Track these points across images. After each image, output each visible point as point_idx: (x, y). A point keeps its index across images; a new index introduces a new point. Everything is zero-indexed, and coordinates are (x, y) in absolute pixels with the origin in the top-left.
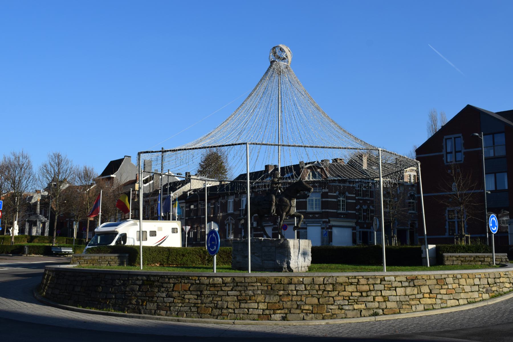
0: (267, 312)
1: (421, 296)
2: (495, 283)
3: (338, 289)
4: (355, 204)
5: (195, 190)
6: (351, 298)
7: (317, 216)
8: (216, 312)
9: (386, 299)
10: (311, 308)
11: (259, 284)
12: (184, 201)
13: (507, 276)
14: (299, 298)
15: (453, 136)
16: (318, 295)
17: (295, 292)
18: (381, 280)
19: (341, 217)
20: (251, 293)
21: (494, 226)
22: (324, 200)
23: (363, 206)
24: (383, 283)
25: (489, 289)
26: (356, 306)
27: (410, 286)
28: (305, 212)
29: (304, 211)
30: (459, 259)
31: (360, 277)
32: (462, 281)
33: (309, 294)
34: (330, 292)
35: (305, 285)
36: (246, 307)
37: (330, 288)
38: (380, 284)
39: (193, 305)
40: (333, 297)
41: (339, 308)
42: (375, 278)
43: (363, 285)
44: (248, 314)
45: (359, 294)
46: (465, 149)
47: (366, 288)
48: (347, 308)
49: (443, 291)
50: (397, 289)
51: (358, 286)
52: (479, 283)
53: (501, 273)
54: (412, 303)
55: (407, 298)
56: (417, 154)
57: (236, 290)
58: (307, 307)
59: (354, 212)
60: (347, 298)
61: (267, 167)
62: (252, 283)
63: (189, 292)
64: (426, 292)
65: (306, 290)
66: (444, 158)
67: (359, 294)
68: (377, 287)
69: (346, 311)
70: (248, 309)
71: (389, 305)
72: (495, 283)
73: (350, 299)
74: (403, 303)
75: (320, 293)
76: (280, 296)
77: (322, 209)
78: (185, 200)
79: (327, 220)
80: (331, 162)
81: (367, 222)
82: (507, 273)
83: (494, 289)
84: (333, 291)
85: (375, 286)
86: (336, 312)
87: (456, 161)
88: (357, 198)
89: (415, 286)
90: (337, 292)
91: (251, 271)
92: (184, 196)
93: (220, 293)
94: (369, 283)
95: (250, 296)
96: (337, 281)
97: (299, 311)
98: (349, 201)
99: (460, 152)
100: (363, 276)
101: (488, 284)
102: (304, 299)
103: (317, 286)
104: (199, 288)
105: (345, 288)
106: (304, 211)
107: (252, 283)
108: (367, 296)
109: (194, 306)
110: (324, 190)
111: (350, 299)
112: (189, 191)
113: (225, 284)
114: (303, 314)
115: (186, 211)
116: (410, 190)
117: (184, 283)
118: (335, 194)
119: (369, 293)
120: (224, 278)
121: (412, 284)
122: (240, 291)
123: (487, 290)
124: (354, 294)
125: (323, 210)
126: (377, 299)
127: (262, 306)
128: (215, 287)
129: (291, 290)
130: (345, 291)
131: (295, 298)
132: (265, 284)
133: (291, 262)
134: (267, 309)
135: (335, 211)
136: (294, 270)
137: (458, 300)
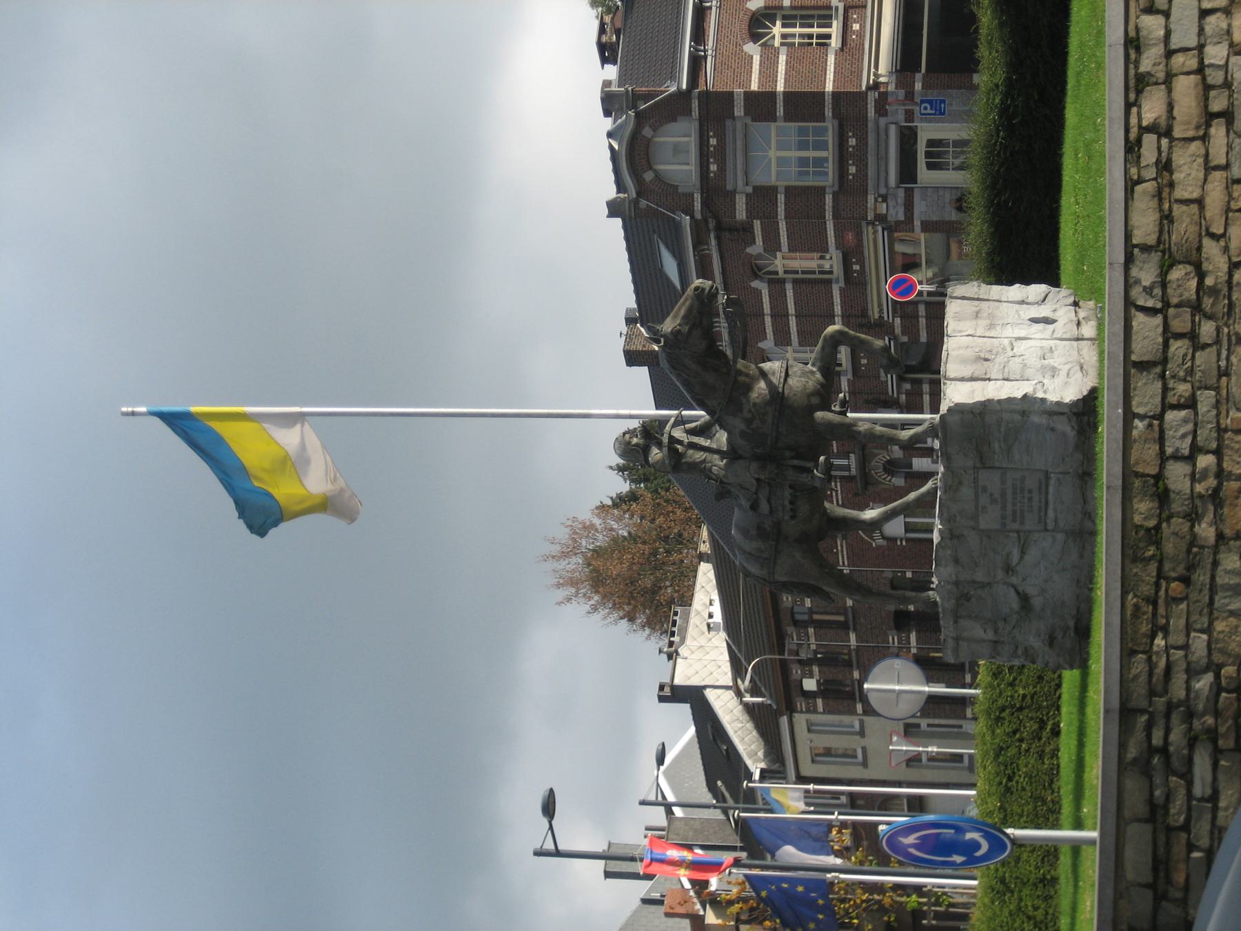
5: (738, 669)
7: (852, 142)
11: (1159, 642)
12: (784, 720)
16: (1218, 342)
17: (1205, 461)
19: (861, 34)
20: (1203, 684)
28: (835, 194)
29: (829, 199)
33: (1217, 389)
35: (1166, 407)
38: (1167, 14)
42: (1133, 44)
43: (1170, 106)
45: (1218, 131)
47: (1185, 87)
51: (1177, 133)
57: (1190, 761)
61: (633, 358)
62: (1151, 675)
65: (1191, 404)
67: (1218, 131)
68: (1185, 35)
75: (1207, 329)
76: (1220, 536)
77: (822, 118)
78: (777, 714)
80: (611, 72)
85: (1175, 43)
90: (1207, 242)
92: (763, 720)
94: (1161, 76)
100: (1128, 106)
103: (1178, 348)
106: (829, 199)
107: (1151, 675)
110: (739, 111)
112: (739, 694)
113: (1155, 812)
119: (1216, 77)
120: (1127, 814)
122: (1192, 742)
125: (828, 112)
129: (1193, 478)
130: (1200, 202)
132: (1161, 610)
133: (1052, 397)
135: (831, 59)
136: (1089, 383)
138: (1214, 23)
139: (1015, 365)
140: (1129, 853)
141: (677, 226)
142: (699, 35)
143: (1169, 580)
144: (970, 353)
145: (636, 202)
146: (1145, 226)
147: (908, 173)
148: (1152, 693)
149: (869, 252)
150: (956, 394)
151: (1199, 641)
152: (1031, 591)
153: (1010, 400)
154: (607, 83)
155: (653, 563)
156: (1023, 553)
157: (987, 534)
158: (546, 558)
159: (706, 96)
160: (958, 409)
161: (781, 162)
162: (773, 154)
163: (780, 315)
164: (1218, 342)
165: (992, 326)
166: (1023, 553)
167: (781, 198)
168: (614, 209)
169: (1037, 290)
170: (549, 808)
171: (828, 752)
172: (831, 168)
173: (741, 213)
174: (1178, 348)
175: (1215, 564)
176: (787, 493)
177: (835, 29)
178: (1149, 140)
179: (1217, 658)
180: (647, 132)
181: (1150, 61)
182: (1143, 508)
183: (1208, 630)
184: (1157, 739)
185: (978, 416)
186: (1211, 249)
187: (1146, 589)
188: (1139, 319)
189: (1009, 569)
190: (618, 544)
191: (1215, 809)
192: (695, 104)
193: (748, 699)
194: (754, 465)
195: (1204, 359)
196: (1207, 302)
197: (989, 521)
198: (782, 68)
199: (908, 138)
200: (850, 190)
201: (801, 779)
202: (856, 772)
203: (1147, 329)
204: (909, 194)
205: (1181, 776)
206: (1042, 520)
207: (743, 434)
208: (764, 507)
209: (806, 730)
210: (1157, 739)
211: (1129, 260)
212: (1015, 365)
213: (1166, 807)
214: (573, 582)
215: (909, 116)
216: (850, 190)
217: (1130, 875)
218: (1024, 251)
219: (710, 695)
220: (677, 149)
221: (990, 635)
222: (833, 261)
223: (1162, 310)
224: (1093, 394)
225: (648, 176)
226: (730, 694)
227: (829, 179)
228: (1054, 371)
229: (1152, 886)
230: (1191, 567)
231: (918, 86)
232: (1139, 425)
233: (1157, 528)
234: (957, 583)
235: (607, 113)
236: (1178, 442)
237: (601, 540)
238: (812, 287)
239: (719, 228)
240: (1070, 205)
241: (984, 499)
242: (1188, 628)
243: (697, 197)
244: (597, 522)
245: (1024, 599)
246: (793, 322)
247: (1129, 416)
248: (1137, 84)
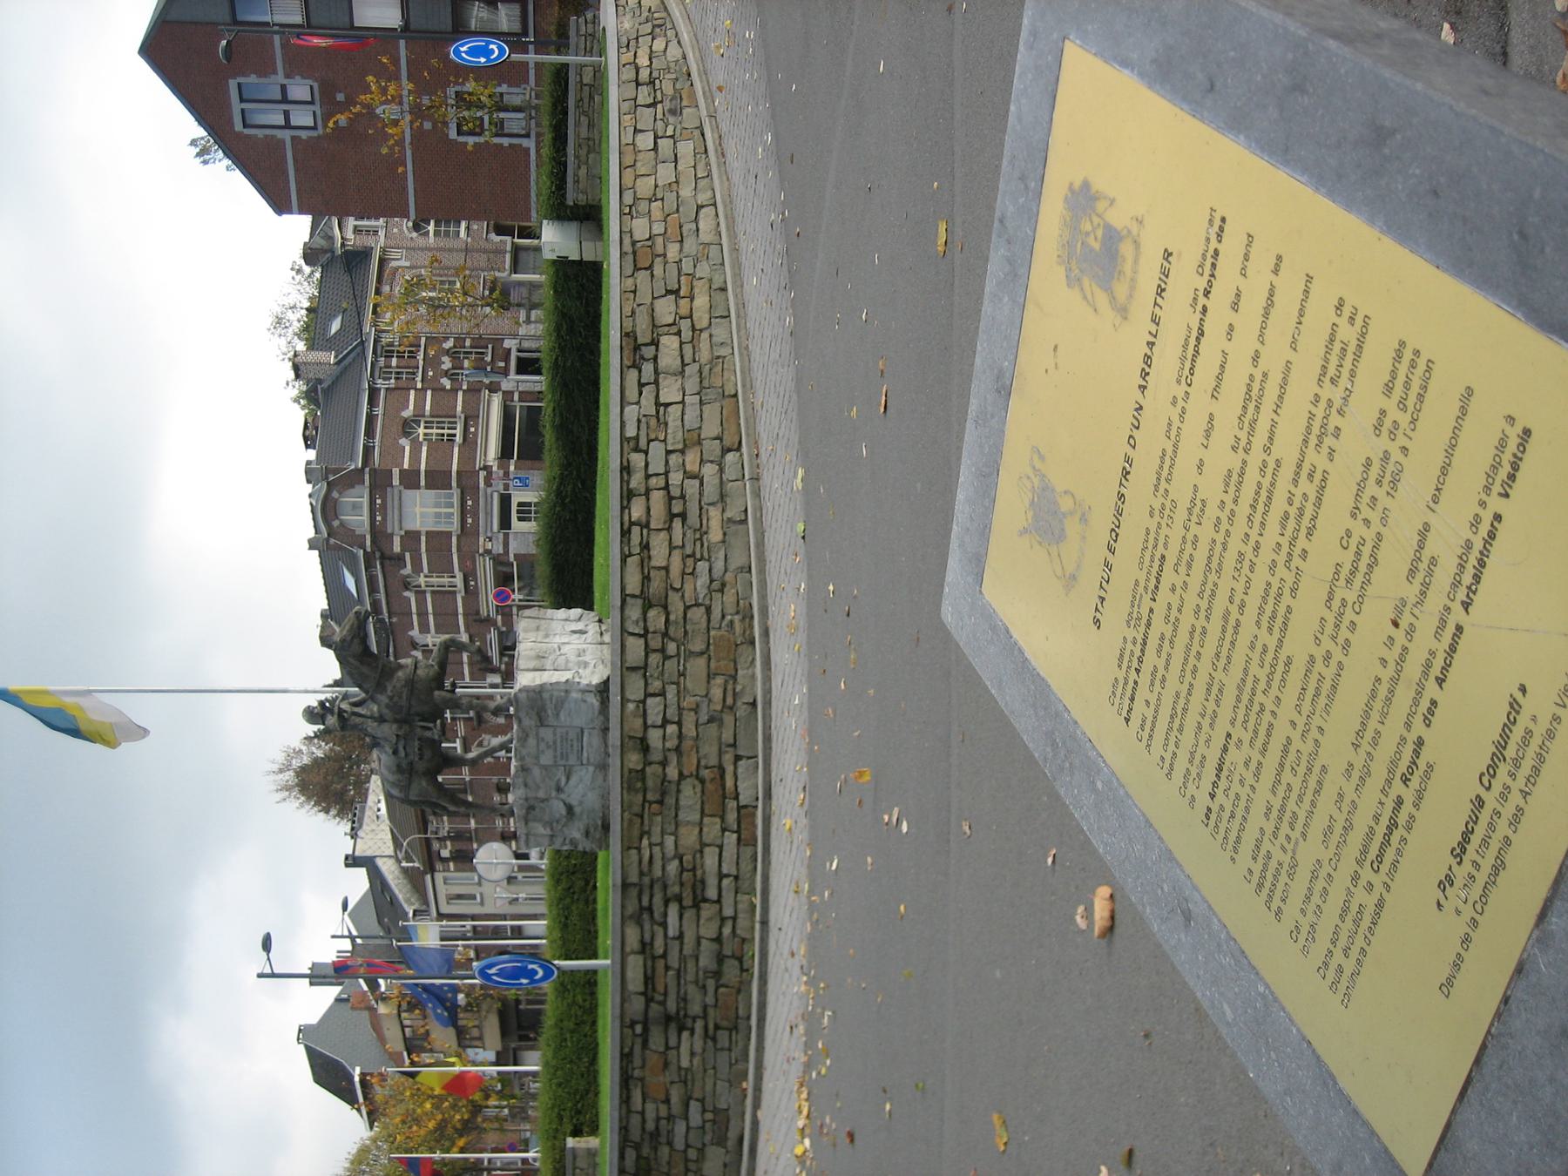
0: (732, 817)
1: (685, 325)
2: (652, 82)
3: (663, 591)
4: (438, 390)
5: (397, 845)
6: (688, 551)
8: (731, 971)
9: (693, 440)
10: (719, 680)
11: (645, 842)
12: (428, 877)
13: (632, 43)
14: (689, 719)
15: (237, 106)
16: (678, 655)
18: (637, 449)
19: (475, 434)
20: (673, 867)
21: (486, 52)
22: (423, 483)
23: (444, 367)
24: (643, 443)
25: (667, 104)
26: (715, 535)
27: (655, 358)
28: (459, 537)
30: (583, 158)
31: (626, 518)
32: (645, 187)
33: (678, 684)
34: (672, 617)
35: (647, 695)
36: (716, 882)
37: (656, 618)
38: (646, 453)
39: (710, 1043)
40: (687, 608)
41: (721, 590)
42: (626, 469)
43: (648, 509)
44: (736, 878)
45: (677, 523)
46: (275, 72)
47: (657, 497)
48: (719, 565)
49: (673, 251)
50: (662, 400)
52: (651, 135)
53: (624, 59)
54: (704, 355)
55: (691, 370)
56: (290, 212)
57: (665, 915)
58: (717, 693)
59: (460, 394)
60: (690, 561)
62: (640, 862)
63: (672, 1054)
64: (673, 308)
65: (663, 694)
66: (304, 135)
68: (657, 466)
69: (732, 567)
70: (721, 876)
71: (711, 429)
72: (652, 82)
73: (693, 555)
74: (705, 383)
75: (672, 648)
76: (681, 774)
79: (482, 474)
80: (312, 454)
81: (489, 359)
82: (624, 40)
83: (668, 88)
84: (665, 607)
86: (733, 599)
87: (312, 103)
88: (419, 386)
89: (655, 343)
91: (594, 956)
92: (415, 880)
93: (674, 960)
94: (643, 491)
95: (682, 870)
96: (637, 592)
97: (728, 719)
98: (428, 407)
99: (284, 88)
100: (623, 509)
101: (654, 105)
102: (688, 702)
104: (656, 1017)
105: (659, 568)
107: (640, 862)
108: (683, 497)
109: (714, 1039)
110: (396, 482)
111: (693, 555)
113: (645, 947)
114: (739, 703)
115: (456, 870)
116: (401, 231)
117: (643, 1067)
118: (407, 449)
119: (675, 492)
120: (628, 949)
121: (649, 352)
122: (666, 902)
123: (673, 112)
124: (678, 541)
125: (454, 484)
126: (692, 467)
127: (712, 827)
128: (653, 978)
130: (667, 569)
131: (689, 729)
134: (723, 818)
135: (456, 450)
137: (700, 207)
138: (673, 458)
139: (561, 660)
140: (630, 974)
141: (354, 557)
142: (371, 419)
143: (651, 803)
144: (533, 653)
145: (327, 540)
146: (633, 585)
147: (505, 523)
148: (642, 874)
149: (480, 572)
150: (524, 679)
151: (670, 841)
152: (574, 803)
153: (557, 683)
154: (309, 463)
155: (341, 774)
156: (568, 779)
157: (545, 768)
158: (269, 773)
159: (374, 472)
160: (525, 689)
161: (423, 515)
162: (418, 510)
163: (422, 614)
164: (678, 655)
165: (547, 636)
166: (568, 779)
167: (423, 538)
168: (312, 545)
169: (577, 612)
170: (267, 944)
171: (459, 897)
172: (456, 519)
173: (397, 548)
174: (654, 659)
175: (679, 791)
176: (417, 743)
177: (459, 432)
178: (636, 530)
179: (681, 851)
180: (335, 494)
181: (636, 481)
182: (634, 760)
183: (675, 834)
184: (645, 903)
185: (537, 695)
186: (674, 598)
187: (637, 809)
188: (630, 640)
189: (559, 789)
190: (316, 762)
191: (682, 944)
192: (367, 477)
193: (404, 864)
194: (395, 726)
195: (671, 665)
196: (671, 632)
197: (546, 759)
198: (424, 455)
199: (505, 501)
200: (468, 532)
201: (441, 917)
202: (477, 910)
203: (636, 647)
204: (506, 536)
205: (660, 924)
206: (580, 758)
207: (387, 706)
208: (402, 753)
209: (446, 882)
210: (645, 903)
211: (623, 602)
212: (561, 660)
213: (652, 944)
214: (287, 788)
215: (506, 487)
216: (468, 532)
217: (631, 987)
218: (571, 584)
219: (379, 862)
220: (356, 507)
221: (548, 832)
222: (459, 580)
223: (644, 635)
224: (606, 682)
225: (336, 523)
226: (392, 861)
227: (455, 527)
228: (586, 665)
229: (644, 994)
230: (664, 793)
231: (512, 468)
232: (631, 706)
233: (643, 770)
234: (526, 799)
235: (309, 481)
236: (654, 717)
237: (306, 760)
238: (444, 596)
239: (383, 557)
240: (598, 560)
241: (543, 746)
242: (663, 833)
243: (368, 537)
244: (304, 748)
245: (570, 809)
246: (431, 618)
247: (624, 701)
248: (628, 496)
